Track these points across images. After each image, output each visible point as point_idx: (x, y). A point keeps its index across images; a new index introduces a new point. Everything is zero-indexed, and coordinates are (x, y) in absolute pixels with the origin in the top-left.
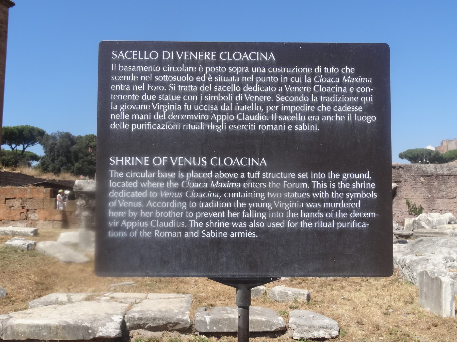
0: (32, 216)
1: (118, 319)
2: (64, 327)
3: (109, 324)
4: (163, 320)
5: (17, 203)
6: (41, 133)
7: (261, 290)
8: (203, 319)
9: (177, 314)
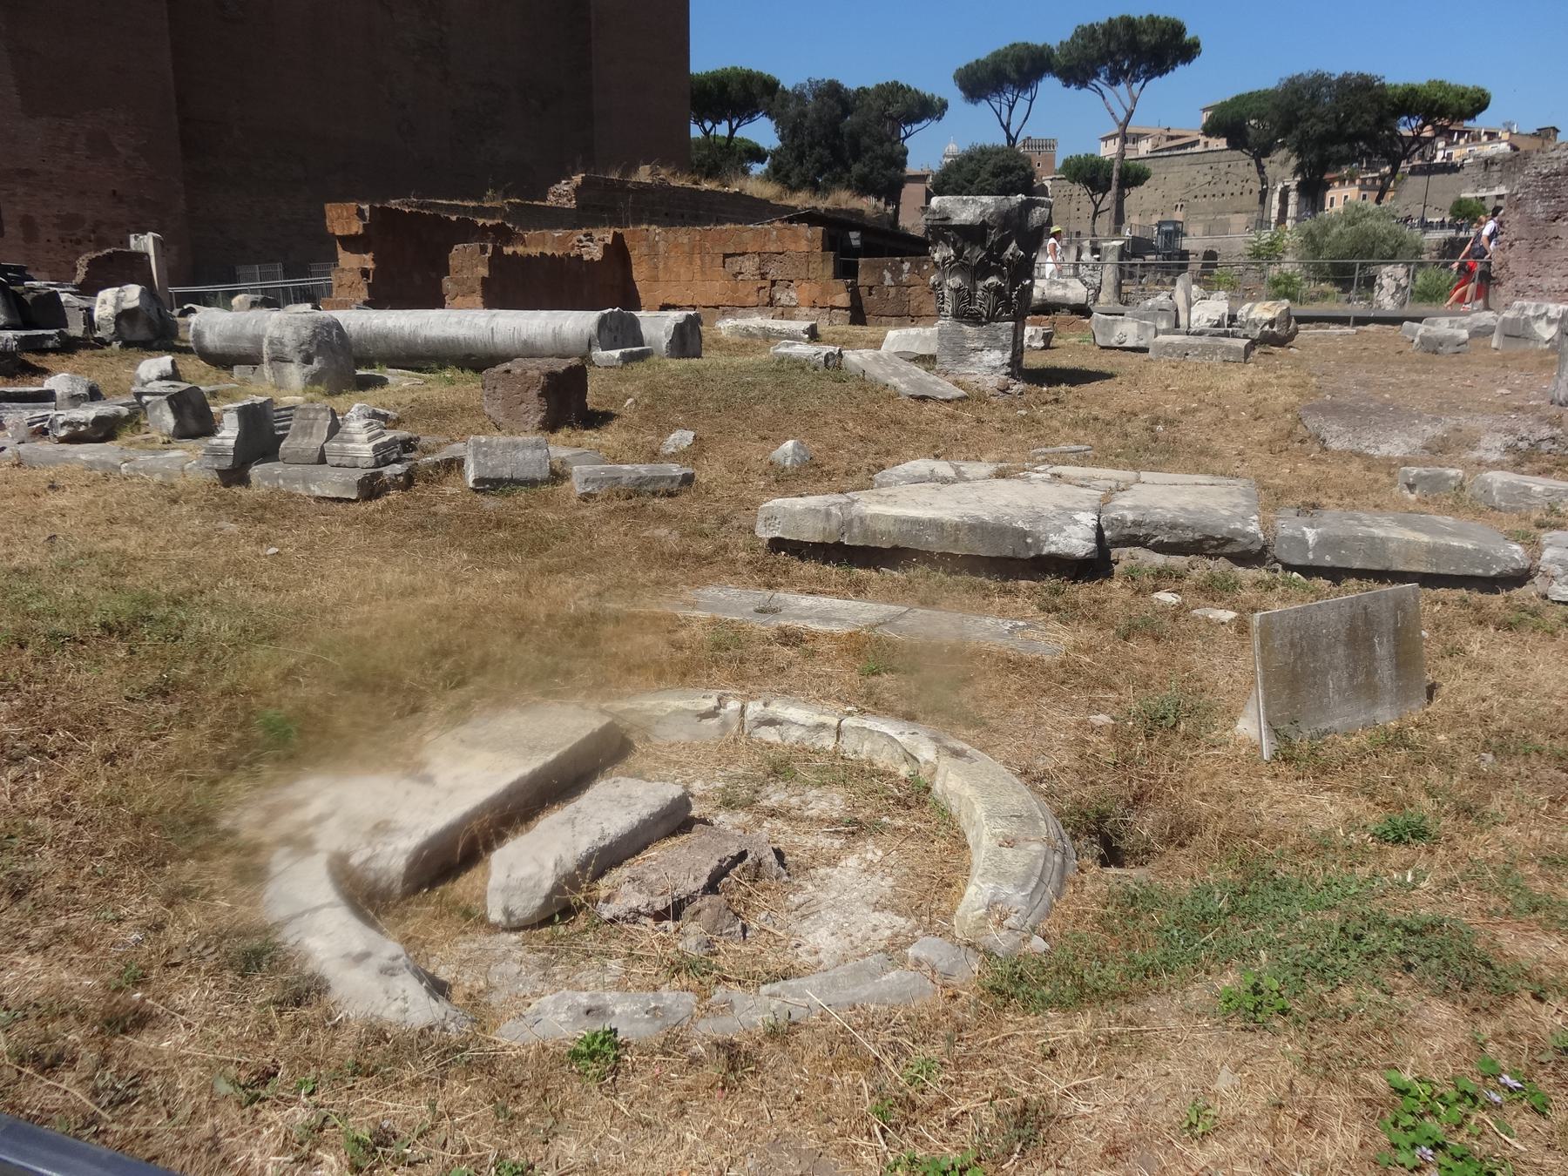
0: (783, 297)
1: (1088, 519)
2: (972, 528)
3: (1070, 529)
4: (1193, 530)
5: (749, 266)
6: (770, 86)
7: (1449, 479)
8: (1298, 534)
9: (1228, 519)
